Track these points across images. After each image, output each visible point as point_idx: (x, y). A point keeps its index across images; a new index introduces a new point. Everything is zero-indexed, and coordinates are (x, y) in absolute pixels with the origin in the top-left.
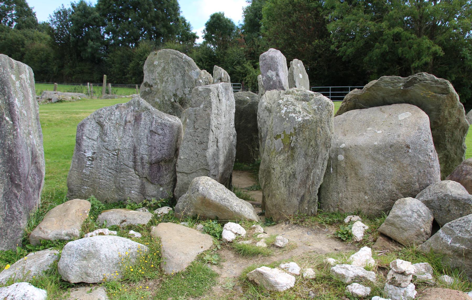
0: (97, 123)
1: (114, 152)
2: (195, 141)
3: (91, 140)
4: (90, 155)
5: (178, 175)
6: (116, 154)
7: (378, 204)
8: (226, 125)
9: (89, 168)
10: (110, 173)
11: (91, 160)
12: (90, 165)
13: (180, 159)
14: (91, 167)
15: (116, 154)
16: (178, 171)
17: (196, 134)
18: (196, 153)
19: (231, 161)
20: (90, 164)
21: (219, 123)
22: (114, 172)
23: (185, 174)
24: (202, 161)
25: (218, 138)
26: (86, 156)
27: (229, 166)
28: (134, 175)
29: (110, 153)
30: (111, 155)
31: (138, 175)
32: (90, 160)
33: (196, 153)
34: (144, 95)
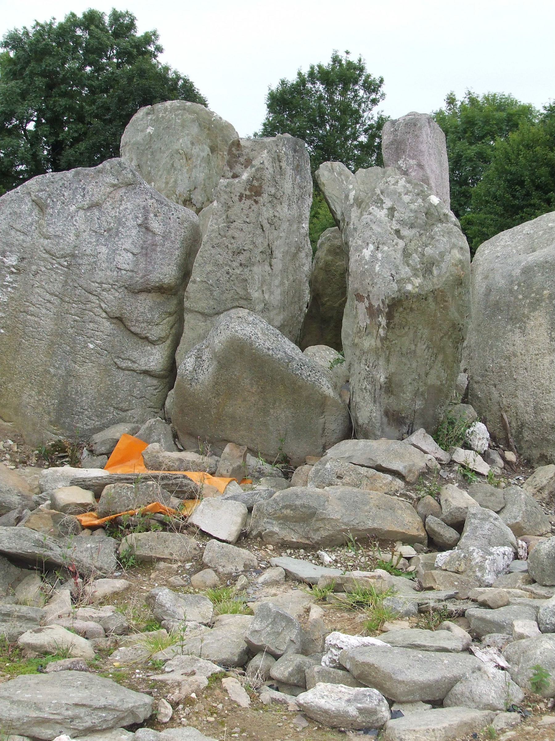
0: (33, 201)
1: (63, 260)
2: (227, 247)
3: (19, 233)
4: (14, 263)
5: (187, 317)
6: (66, 263)
7: (275, 605)
8: (290, 225)
9: (9, 289)
10: (49, 302)
11: (15, 273)
12: (11, 283)
13: (194, 282)
14: (13, 288)
15: (66, 263)
16: (187, 308)
17: (230, 233)
18: (228, 273)
19: (297, 307)
20: (11, 280)
21: (276, 214)
22: (57, 301)
23: (200, 317)
24: (238, 290)
25: (274, 249)
26: (6, 265)
27: (292, 317)
28: (97, 312)
29: (55, 262)
30: (56, 265)
31: (106, 312)
32: (12, 273)
33: (228, 273)
34: (206, 497)
